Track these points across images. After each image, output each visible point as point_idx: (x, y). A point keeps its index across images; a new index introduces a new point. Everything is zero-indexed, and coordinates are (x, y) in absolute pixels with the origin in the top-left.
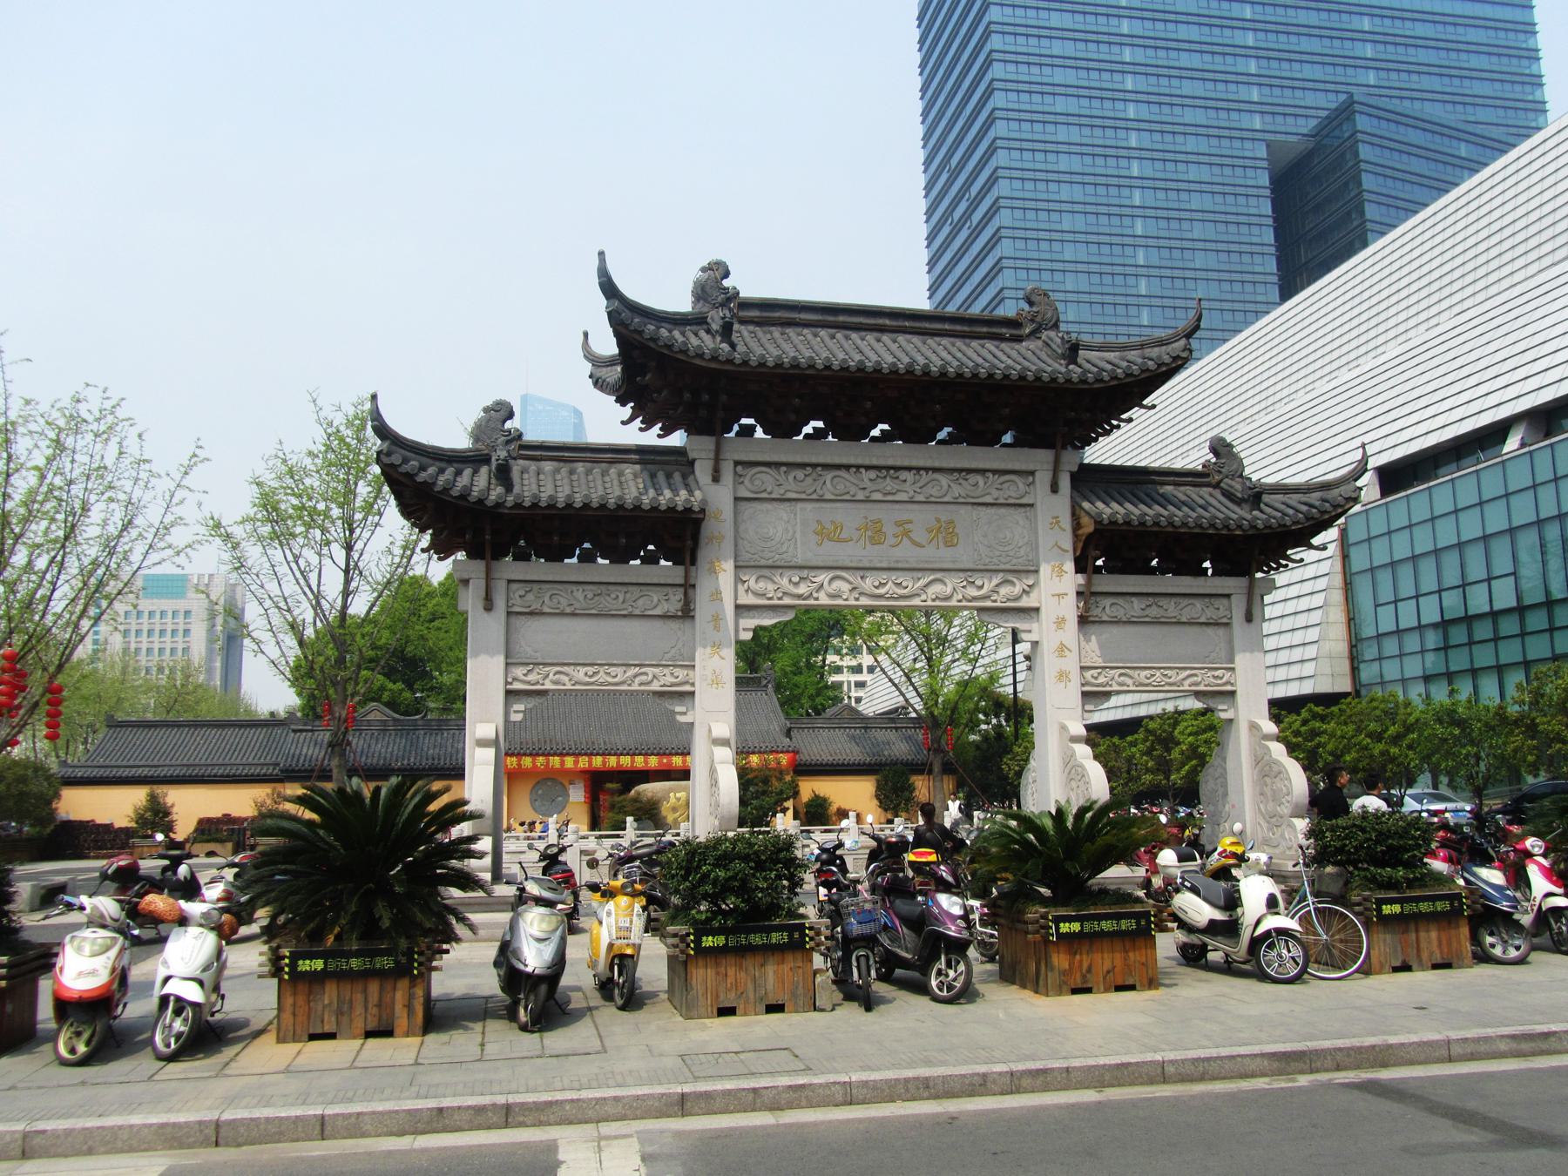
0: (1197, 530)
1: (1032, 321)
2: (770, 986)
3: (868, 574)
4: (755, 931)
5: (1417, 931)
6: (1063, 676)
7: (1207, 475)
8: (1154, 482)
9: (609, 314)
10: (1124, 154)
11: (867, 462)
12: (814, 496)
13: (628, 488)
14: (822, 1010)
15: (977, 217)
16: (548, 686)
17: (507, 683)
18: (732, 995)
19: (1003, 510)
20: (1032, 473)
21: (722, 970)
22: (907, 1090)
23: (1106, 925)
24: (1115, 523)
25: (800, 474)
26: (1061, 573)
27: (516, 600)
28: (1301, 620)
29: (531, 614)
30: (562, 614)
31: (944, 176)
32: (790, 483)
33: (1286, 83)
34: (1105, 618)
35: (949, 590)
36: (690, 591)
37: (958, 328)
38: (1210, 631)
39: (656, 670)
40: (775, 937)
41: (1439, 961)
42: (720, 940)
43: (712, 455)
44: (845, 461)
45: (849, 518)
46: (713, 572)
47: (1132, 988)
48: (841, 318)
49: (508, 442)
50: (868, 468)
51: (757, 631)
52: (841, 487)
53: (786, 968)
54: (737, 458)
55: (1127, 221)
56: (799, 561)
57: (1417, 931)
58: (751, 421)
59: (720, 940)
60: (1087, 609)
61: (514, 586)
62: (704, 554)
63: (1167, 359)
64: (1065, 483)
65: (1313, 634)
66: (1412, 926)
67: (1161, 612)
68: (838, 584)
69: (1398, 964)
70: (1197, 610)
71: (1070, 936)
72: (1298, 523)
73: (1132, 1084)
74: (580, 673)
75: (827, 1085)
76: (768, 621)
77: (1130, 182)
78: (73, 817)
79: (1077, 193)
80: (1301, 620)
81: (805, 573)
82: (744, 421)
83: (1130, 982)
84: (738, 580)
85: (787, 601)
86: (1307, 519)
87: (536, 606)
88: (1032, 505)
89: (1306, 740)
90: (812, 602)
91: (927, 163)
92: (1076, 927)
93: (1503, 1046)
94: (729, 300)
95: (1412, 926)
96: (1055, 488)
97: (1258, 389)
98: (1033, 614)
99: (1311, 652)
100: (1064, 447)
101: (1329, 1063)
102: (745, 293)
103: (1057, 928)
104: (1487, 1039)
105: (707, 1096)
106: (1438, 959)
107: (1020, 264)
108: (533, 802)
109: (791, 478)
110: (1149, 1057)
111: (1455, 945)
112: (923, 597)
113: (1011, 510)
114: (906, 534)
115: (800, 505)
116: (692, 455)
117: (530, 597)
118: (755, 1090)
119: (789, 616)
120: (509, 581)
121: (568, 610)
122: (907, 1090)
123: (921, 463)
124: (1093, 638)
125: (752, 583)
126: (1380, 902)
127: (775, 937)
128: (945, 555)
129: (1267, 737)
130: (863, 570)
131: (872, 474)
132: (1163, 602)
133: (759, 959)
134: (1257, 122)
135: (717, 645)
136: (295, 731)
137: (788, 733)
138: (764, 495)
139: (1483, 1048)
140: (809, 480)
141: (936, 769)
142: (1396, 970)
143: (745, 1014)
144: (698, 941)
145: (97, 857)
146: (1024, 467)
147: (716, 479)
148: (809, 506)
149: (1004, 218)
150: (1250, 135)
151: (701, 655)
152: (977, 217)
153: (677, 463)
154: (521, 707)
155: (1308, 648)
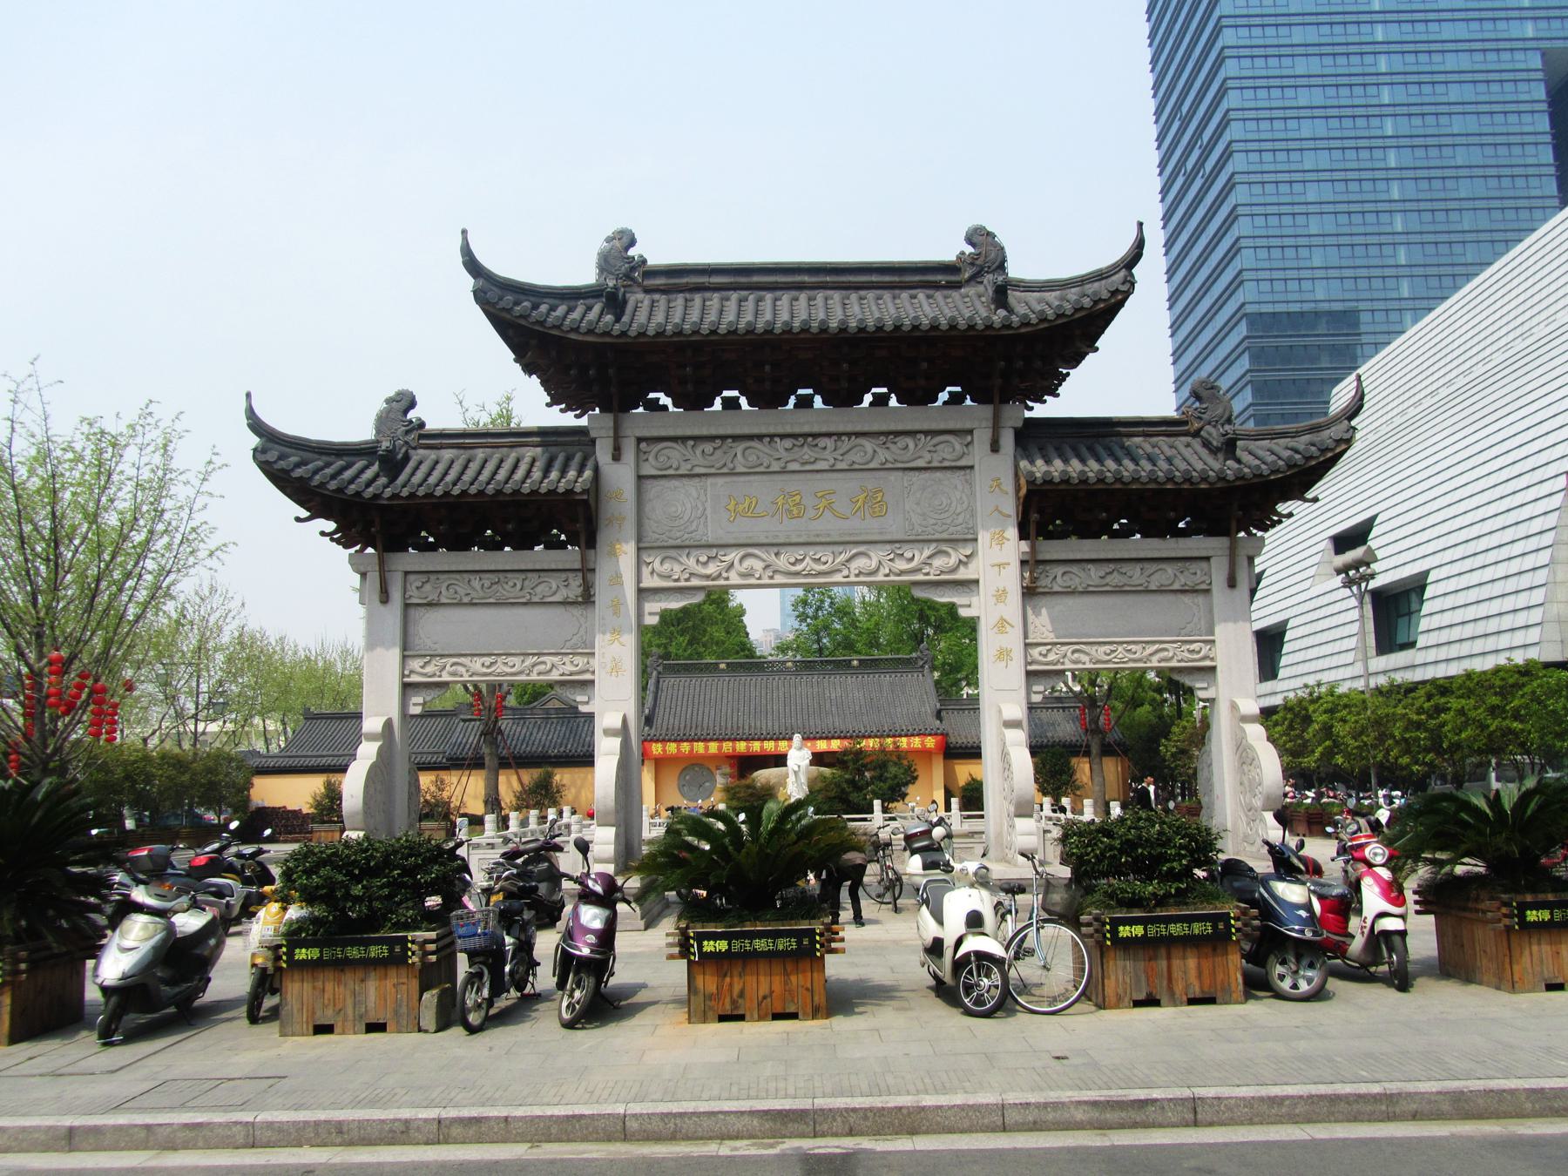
0: (1118, 486)
1: (972, 264)
2: (371, 1005)
3: (783, 550)
4: (353, 943)
5: (1169, 958)
6: (1003, 654)
7: (1185, 423)
8: (1120, 434)
9: (475, 293)
10: (1372, 80)
11: (780, 430)
12: (725, 470)
13: (527, 473)
14: (426, 1031)
15: (1209, 165)
16: (446, 678)
17: (403, 676)
18: (329, 1012)
19: (938, 474)
20: (971, 432)
21: (319, 984)
22: (317, 1134)
23: (761, 945)
24: (1051, 482)
25: (708, 447)
26: (1001, 540)
27: (412, 591)
28: (1525, 581)
29: (430, 605)
30: (460, 604)
31: (1176, 125)
32: (697, 458)
34: (1056, 588)
35: (874, 564)
36: (589, 575)
37: (887, 278)
38: (1186, 599)
39: (555, 659)
40: (374, 951)
41: (1198, 994)
42: (314, 953)
43: (611, 433)
44: (756, 431)
45: (762, 490)
46: (613, 554)
47: (793, 1016)
48: (755, 279)
49: (407, 432)
50: (783, 436)
51: (665, 616)
52: (752, 458)
53: (389, 983)
54: (639, 434)
55: (1378, 154)
56: (711, 541)
57: (1169, 958)
58: (735, 393)
59: (314, 953)
60: (1034, 580)
61: (411, 577)
62: (602, 538)
63: (1105, 295)
64: (1008, 440)
65: (1538, 596)
66: (1163, 952)
67: (1124, 580)
68: (749, 562)
69: (1142, 996)
70: (1166, 575)
71: (1131, 942)
72: (1278, 471)
73: (585, 1139)
74: (477, 665)
75: (229, 1125)
76: (675, 604)
77: (1383, 111)
78: (268, 803)
79: (1320, 128)
80: (1525, 581)
81: (713, 552)
82: (726, 393)
83: (792, 1009)
84: (639, 563)
85: (695, 582)
86: (1290, 467)
87: (433, 597)
88: (972, 467)
89: (1430, 717)
90: (722, 582)
91: (1158, 113)
92: (722, 945)
93: (1079, 1115)
94: (633, 269)
95: (1163, 952)
96: (995, 447)
97: (1512, 326)
98: (973, 587)
99: (1536, 616)
100: (1005, 401)
101: (838, 1124)
102: (652, 261)
103: (700, 947)
104: (1057, 1105)
105: (96, 1130)
106: (1196, 991)
107: (1256, 210)
108: (681, 788)
109: (698, 452)
110: (608, 1109)
111: (1220, 977)
112: (845, 572)
113: (948, 474)
114: (829, 506)
115: (710, 480)
116: (593, 434)
117: (428, 587)
118: (148, 1127)
119: (698, 598)
120: (407, 573)
121: (466, 600)
122: (317, 1134)
123: (841, 429)
124: (1044, 611)
125: (657, 565)
126: (1116, 923)
127: (374, 951)
128: (870, 526)
129: (1246, 719)
130: (777, 546)
131: (788, 443)
132: (1125, 568)
133: (360, 974)
134: (1529, 30)
135: (617, 631)
136: (465, 721)
137: (938, 715)
138: (671, 472)
139: (1050, 1116)
140: (719, 453)
141: (1095, 750)
142: (1138, 1004)
143: (343, 1033)
144: (290, 954)
145: (285, 842)
146: (959, 426)
147: (617, 456)
148: (720, 481)
149: (1238, 163)
150: (1521, 45)
151: (601, 642)
152: (1209, 165)
153: (579, 443)
154: (420, 700)
155: (1533, 611)
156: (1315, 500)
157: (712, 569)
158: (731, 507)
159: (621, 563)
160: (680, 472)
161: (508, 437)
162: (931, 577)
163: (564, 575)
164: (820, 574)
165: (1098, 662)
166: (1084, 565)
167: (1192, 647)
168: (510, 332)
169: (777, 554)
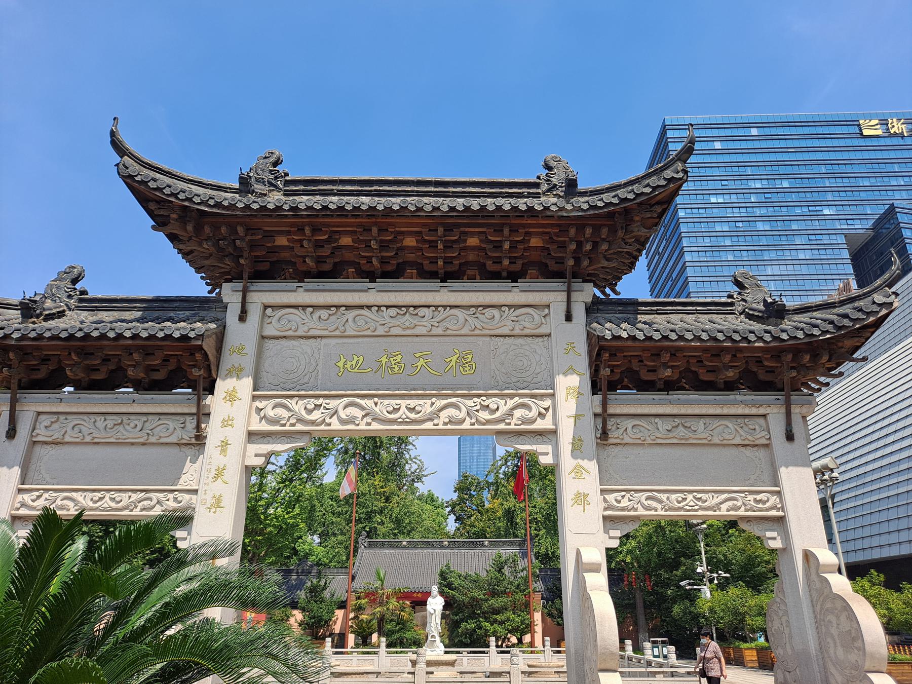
6: (581, 498)
12: (337, 333)
19: (520, 341)
25: (324, 314)
31: (670, 283)
34: (627, 440)
61: (42, 417)
64: (579, 312)
85: (299, 427)
87: (57, 436)
88: (549, 335)
96: (569, 318)
121: (88, 439)
131: (393, 312)
132: (689, 422)
140: (333, 318)
156: (865, 359)
157: (316, 415)
158: (341, 364)
159: (232, 404)
160: (298, 333)
161: (160, 307)
162: (512, 427)
163: (182, 419)
164: (413, 422)
165: (670, 509)
166: (653, 419)
167: (758, 497)
168: (152, 206)
169: (376, 404)
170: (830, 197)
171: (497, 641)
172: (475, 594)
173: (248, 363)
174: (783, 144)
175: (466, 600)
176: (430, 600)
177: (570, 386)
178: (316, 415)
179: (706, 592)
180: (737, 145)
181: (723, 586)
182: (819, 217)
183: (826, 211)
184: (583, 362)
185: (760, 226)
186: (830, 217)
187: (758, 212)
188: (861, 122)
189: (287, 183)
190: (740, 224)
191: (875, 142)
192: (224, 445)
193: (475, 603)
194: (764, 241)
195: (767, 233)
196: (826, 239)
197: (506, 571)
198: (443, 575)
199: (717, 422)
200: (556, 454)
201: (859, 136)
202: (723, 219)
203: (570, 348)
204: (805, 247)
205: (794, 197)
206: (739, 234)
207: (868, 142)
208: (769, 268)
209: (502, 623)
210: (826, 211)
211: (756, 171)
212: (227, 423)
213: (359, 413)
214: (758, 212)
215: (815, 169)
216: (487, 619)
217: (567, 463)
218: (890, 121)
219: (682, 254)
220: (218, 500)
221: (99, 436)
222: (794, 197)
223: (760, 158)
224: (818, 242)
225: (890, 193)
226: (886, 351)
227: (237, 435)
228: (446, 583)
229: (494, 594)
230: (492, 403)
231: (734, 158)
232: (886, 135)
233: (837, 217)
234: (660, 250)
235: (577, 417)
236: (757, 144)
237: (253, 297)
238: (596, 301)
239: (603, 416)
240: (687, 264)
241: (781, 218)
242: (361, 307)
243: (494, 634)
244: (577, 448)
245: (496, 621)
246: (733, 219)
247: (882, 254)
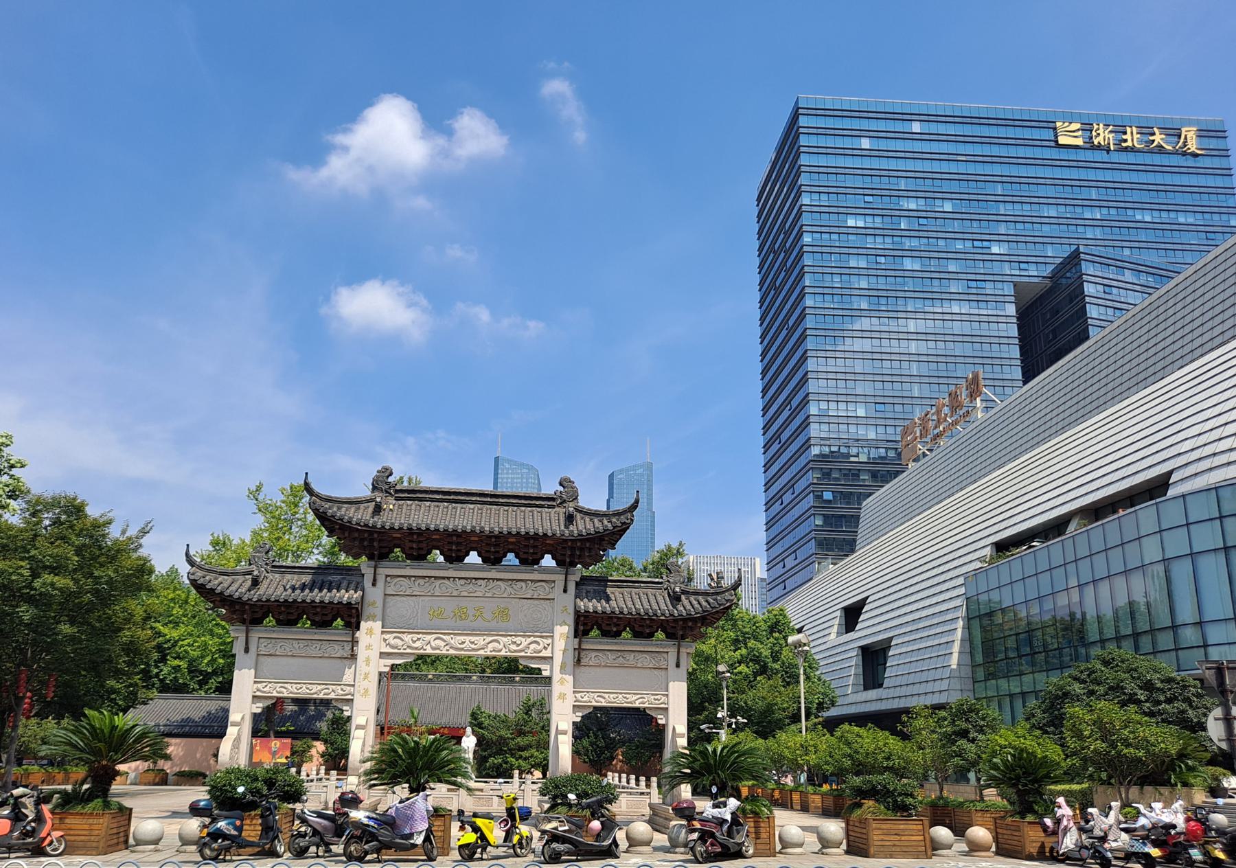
19: (536, 602)
25: (421, 581)
31: (784, 332)
33: (1028, 239)
64: (572, 587)
85: (409, 651)
96: (565, 591)
131: (462, 582)
157: (418, 644)
159: (371, 636)
170: (1002, 229)
171: (520, 774)
172: (503, 733)
173: (378, 611)
174: (952, 148)
175: (495, 738)
176: (464, 739)
177: (563, 632)
178: (418, 644)
179: (723, 734)
180: (892, 145)
181: (739, 728)
182: (986, 257)
183: (995, 249)
184: (571, 619)
185: (908, 264)
186: (998, 258)
187: (907, 244)
188: (1058, 124)
189: (397, 491)
190: (882, 260)
191: (1072, 155)
192: (368, 661)
193: (503, 741)
194: (910, 285)
195: (916, 274)
196: (989, 288)
197: (534, 713)
198: (474, 716)
199: (641, 655)
200: (551, 671)
201: (1053, 144)
202: (861, 251)
203: (565, 610)
204: (962, 297)
205: (956, 226)
206: (879, 273)
207: (1064, 154)
208: (912, 322)
209: (525, 759)
210: (995, 249)
211: (912, 185)
212: (369, 647)
213: (443, 644)
214: (907, 244)
215: (989, 189)
216: (513, 755)
217: (557, 676)
218: (1096, 127)
219: (802, 296)
220: (366, 690)
221: (295, 652)
222: (956, 226)
223: (919, 166)
224: (979, 291)
225: (1080, 229)
226: (1000, 467)
227: (375, 655)
228: (476, 722)
229: (521, 733)
230: (518, 640)
231: (884, 164)
232: (1088, 145)
233: (1007, 258)
234: (778, 284)
235: (565, 651)
236: (918, 146)
237: (380, 571)
238: (583, 578)
239: (579, 650)
240: (808, 311)
241: (935, 255)
242: (443, 578)
243: (519, 768)
244: (563, 669)
245: (521, 757)
246: (873, 252)
247: (1058, 312)
